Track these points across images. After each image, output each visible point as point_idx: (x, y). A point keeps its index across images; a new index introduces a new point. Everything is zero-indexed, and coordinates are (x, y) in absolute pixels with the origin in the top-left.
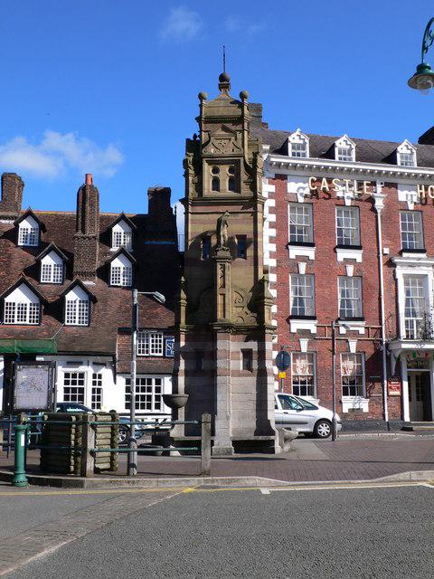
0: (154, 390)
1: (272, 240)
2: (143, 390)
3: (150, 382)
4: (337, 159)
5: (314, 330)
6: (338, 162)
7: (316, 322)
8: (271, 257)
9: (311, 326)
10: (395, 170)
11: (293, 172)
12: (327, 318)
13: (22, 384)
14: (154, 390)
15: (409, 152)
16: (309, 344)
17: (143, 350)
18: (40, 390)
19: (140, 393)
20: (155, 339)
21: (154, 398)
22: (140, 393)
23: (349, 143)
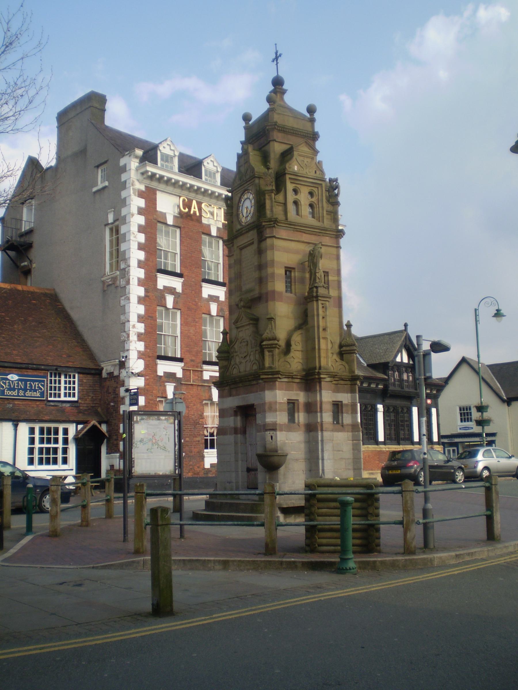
0: (61, 441)
1: (141, 264)
2: (49, 441)
3: (56, 432)
4: (204, 179)
5: (180, 375)
6: (204, 183)
7: (182, 364)
8: (139, 285)
9: (177, 368)
10: (154, 170)
11: (162, 186)
12: (192, 360)
13: (141, 441)
14: (61, 441)
15: (215, 168)
16: (176, 388)
17: (70, 393)
18: (164, 449)
19: (45, 445)
20: (68, 379)
21: (60, 451)
22: (45, 445)
23: (215, 164)
